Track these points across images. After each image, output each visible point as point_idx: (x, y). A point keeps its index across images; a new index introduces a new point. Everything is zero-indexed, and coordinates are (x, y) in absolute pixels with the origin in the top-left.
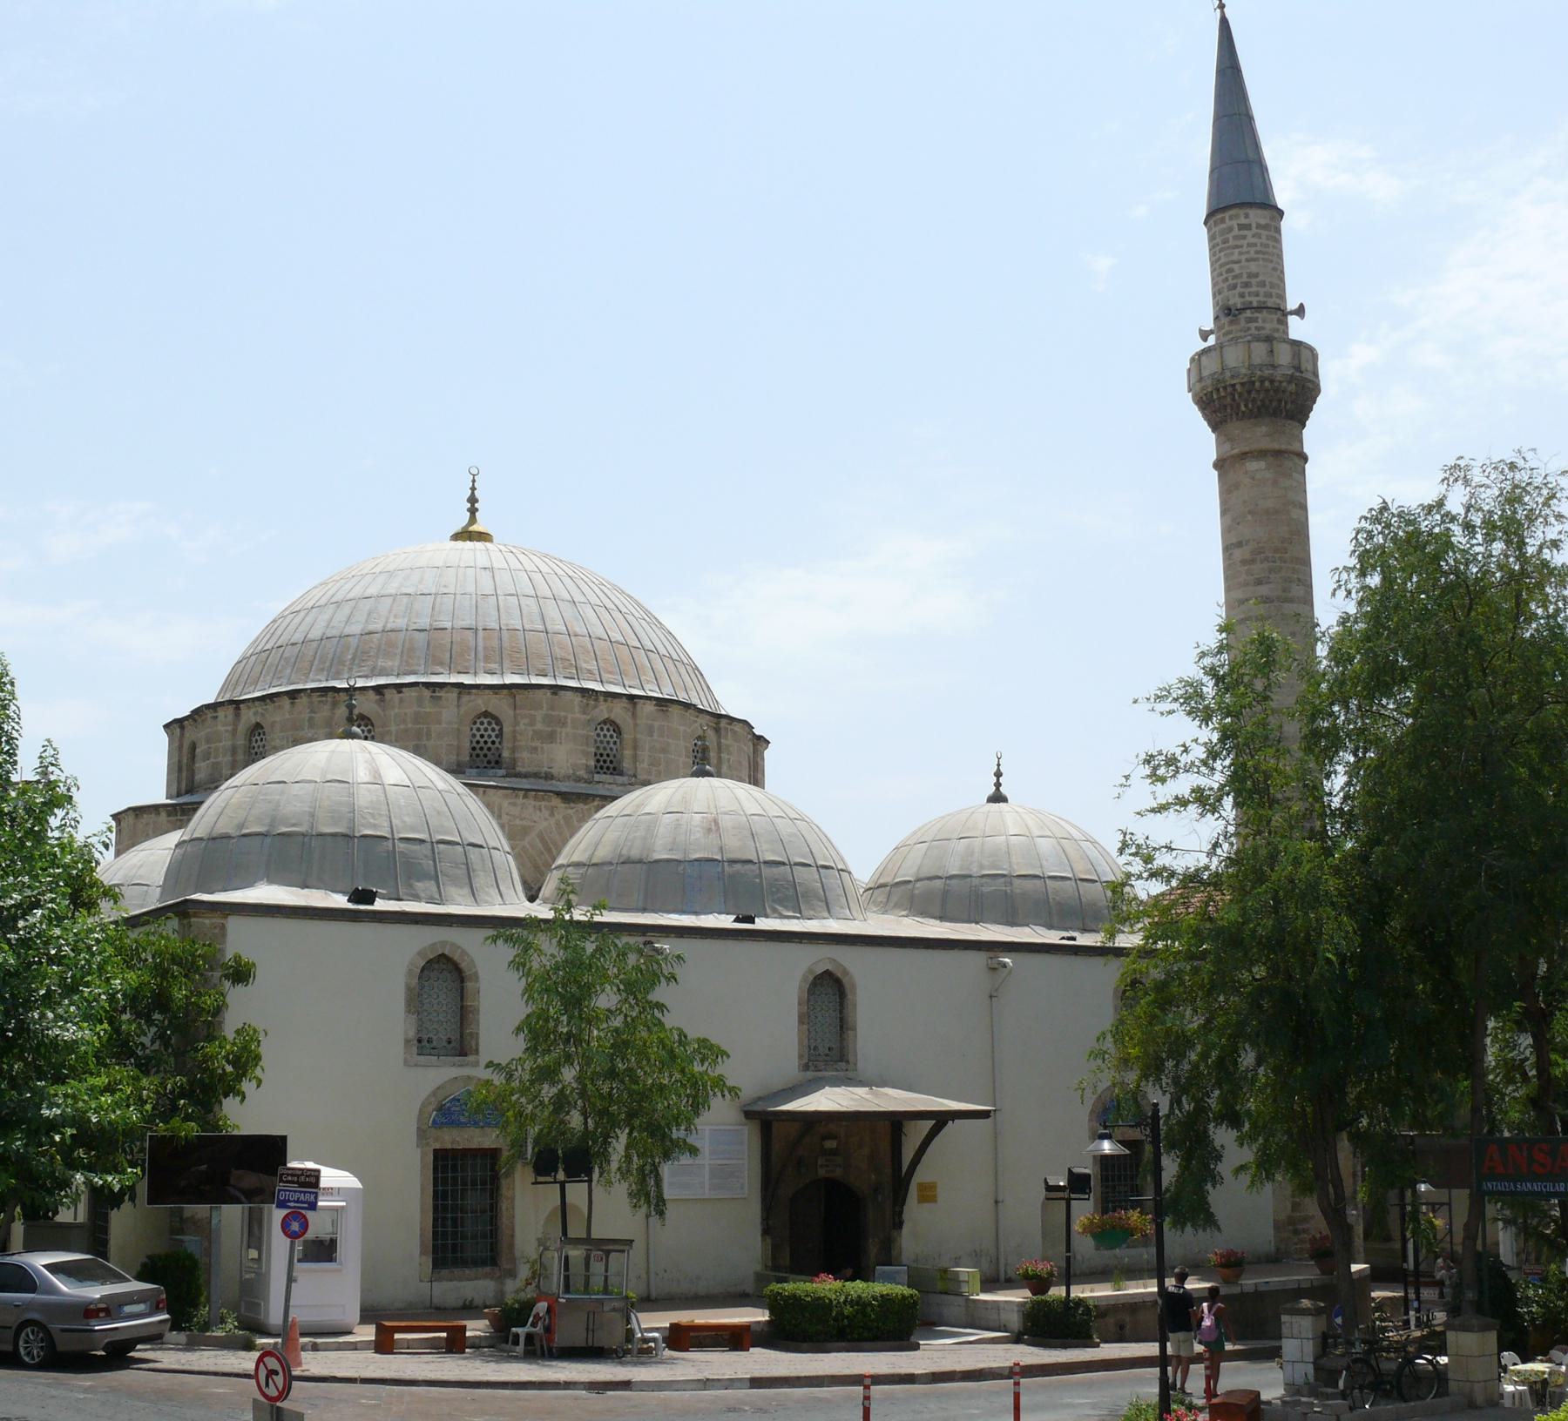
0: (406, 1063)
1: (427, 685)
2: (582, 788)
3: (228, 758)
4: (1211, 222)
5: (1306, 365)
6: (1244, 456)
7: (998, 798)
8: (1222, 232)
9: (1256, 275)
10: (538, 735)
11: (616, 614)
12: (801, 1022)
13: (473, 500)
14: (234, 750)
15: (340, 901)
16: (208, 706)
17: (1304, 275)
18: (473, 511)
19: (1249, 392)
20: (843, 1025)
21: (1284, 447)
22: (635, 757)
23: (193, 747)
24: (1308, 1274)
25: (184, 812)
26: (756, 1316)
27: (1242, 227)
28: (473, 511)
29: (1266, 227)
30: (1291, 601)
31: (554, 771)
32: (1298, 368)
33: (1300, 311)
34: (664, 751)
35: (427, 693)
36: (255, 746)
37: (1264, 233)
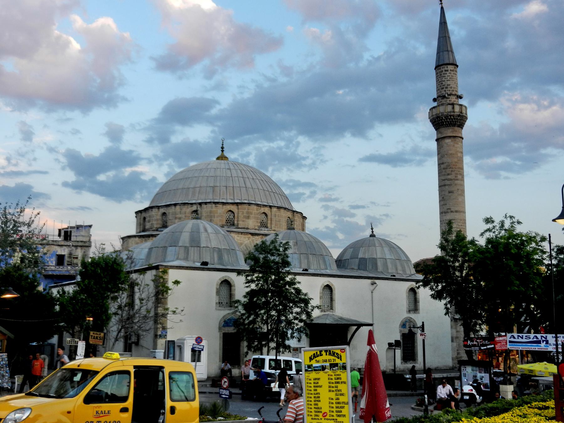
0: (216, 309)
1: (214, 203)
2: (257, 232)
5: (464, 112)
7: (222, 158)
9: (450, 85)
10: (245, 217)
11: (265, 182)
12: (320, 298)
13: (222, 148)
18: (222, 151)
19: (447, 119)
22: (271, 223)
24: (294, 416)
28: (222, 151)
29: (453, 71)
30: (457, 180)
31: (249, 227)
32: (461, 113)
34: (279, 221)
35: (214, 205)
37: (452, 72)
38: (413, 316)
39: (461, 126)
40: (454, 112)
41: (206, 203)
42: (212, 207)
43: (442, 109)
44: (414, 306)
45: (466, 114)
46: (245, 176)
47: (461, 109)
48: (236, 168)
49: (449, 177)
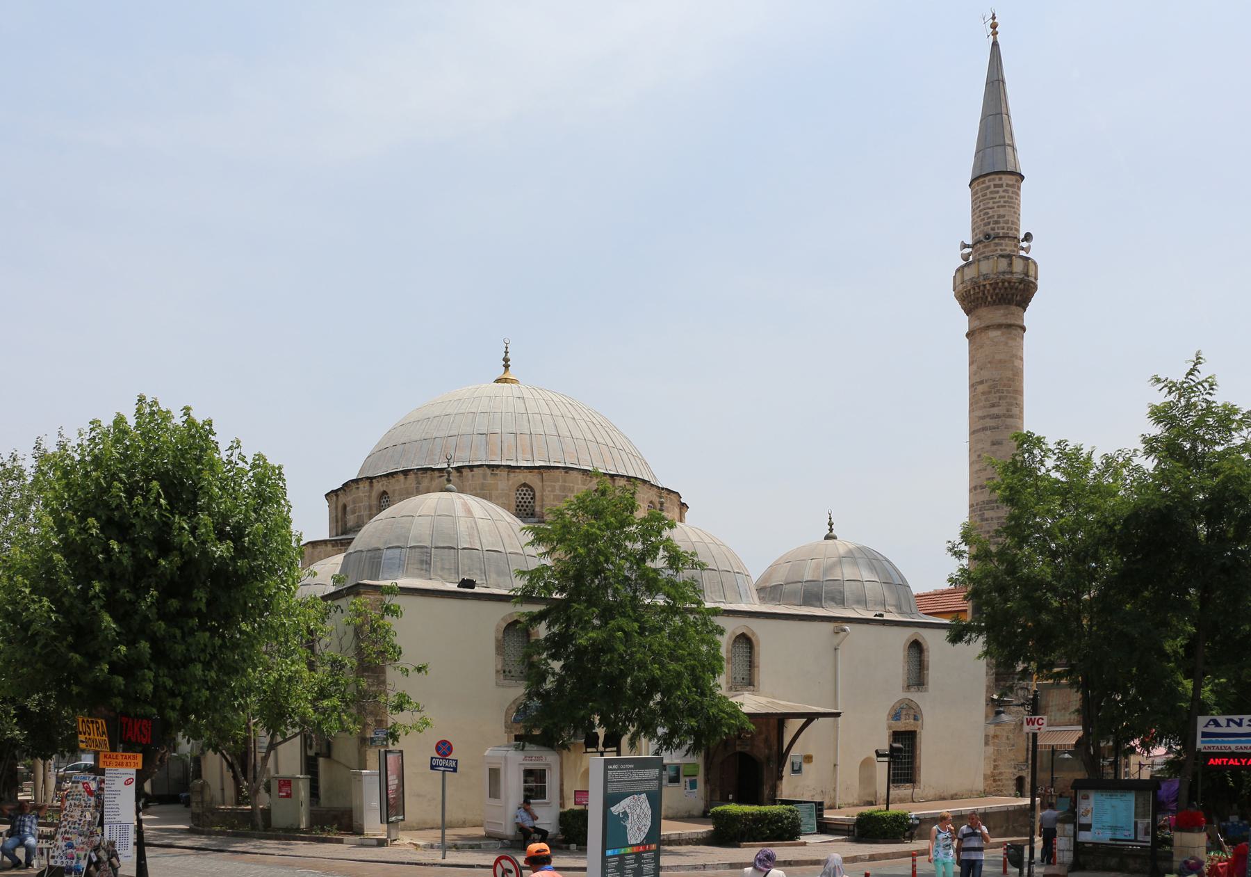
1: (489, 466)
3: (367, 512)
4: (975, 184)
5: (1032, 273)
6: (988, 328)
8: (982, 190)
13: (506, 360)
14: (370, 508)
15: (453, 587)
16: (352, 481)
17: (1034, 211)
18: (507, 367)
20: (751, 665)
21: (1013, 322)
23: (345, 507)
25: (342, 545)
26: (704, 828)
27: (995, 186)
28: (507, 367)
29: (1012, 186)
32: (1027, 274)
33: (1028, 237)
35: (488, 471)
36: (384, 500)
37: (1011, 189)
38: (914, 696)
39: (1024, 303)
40: (1012, 273)
41: (471, 468)
42: (485, 476)
43: (986, 267)
44: (918, 675)
45: (1036, 279)
46: (556, 412)
47: (1027, 266)
48: (537, 396)
49: (995, 411)
